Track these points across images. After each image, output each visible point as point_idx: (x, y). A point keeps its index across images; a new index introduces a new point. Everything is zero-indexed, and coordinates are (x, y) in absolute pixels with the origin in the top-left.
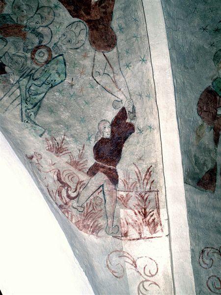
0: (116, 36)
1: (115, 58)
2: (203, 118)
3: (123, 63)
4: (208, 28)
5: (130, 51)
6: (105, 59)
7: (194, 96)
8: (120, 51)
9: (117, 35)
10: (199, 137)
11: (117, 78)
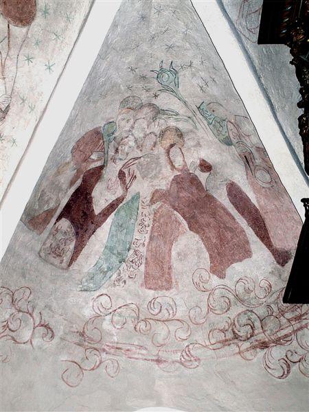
0: (35, 14)
1: (19, 41)
2: (73, 156)
3: (25, 51)
4: (136, 70)
5: (40, 44)
6: (7, 32)
7: (78, 133)
8: (29, 35)
9: (37, 15)
10: (58, 173)
11: (8, 63)
